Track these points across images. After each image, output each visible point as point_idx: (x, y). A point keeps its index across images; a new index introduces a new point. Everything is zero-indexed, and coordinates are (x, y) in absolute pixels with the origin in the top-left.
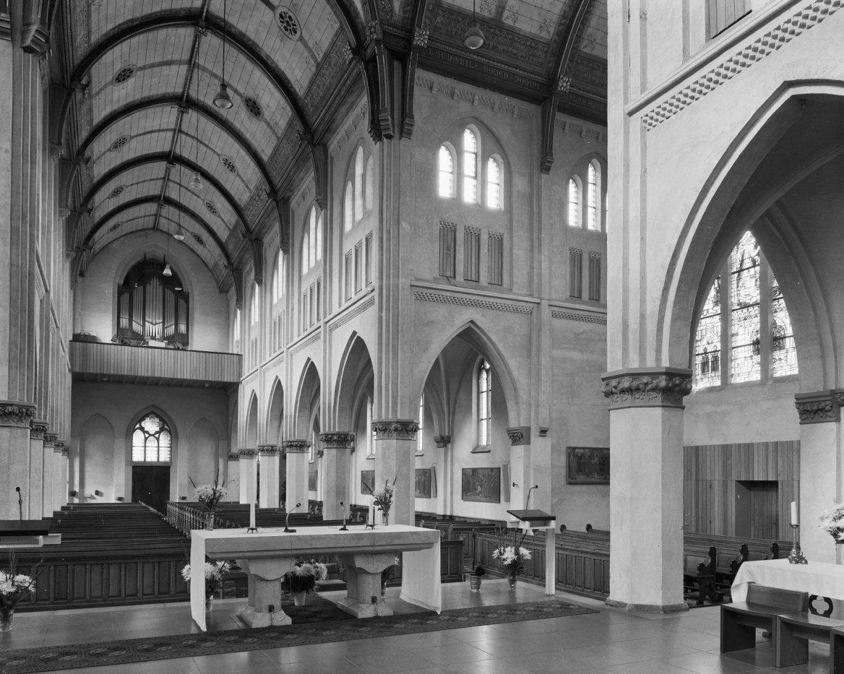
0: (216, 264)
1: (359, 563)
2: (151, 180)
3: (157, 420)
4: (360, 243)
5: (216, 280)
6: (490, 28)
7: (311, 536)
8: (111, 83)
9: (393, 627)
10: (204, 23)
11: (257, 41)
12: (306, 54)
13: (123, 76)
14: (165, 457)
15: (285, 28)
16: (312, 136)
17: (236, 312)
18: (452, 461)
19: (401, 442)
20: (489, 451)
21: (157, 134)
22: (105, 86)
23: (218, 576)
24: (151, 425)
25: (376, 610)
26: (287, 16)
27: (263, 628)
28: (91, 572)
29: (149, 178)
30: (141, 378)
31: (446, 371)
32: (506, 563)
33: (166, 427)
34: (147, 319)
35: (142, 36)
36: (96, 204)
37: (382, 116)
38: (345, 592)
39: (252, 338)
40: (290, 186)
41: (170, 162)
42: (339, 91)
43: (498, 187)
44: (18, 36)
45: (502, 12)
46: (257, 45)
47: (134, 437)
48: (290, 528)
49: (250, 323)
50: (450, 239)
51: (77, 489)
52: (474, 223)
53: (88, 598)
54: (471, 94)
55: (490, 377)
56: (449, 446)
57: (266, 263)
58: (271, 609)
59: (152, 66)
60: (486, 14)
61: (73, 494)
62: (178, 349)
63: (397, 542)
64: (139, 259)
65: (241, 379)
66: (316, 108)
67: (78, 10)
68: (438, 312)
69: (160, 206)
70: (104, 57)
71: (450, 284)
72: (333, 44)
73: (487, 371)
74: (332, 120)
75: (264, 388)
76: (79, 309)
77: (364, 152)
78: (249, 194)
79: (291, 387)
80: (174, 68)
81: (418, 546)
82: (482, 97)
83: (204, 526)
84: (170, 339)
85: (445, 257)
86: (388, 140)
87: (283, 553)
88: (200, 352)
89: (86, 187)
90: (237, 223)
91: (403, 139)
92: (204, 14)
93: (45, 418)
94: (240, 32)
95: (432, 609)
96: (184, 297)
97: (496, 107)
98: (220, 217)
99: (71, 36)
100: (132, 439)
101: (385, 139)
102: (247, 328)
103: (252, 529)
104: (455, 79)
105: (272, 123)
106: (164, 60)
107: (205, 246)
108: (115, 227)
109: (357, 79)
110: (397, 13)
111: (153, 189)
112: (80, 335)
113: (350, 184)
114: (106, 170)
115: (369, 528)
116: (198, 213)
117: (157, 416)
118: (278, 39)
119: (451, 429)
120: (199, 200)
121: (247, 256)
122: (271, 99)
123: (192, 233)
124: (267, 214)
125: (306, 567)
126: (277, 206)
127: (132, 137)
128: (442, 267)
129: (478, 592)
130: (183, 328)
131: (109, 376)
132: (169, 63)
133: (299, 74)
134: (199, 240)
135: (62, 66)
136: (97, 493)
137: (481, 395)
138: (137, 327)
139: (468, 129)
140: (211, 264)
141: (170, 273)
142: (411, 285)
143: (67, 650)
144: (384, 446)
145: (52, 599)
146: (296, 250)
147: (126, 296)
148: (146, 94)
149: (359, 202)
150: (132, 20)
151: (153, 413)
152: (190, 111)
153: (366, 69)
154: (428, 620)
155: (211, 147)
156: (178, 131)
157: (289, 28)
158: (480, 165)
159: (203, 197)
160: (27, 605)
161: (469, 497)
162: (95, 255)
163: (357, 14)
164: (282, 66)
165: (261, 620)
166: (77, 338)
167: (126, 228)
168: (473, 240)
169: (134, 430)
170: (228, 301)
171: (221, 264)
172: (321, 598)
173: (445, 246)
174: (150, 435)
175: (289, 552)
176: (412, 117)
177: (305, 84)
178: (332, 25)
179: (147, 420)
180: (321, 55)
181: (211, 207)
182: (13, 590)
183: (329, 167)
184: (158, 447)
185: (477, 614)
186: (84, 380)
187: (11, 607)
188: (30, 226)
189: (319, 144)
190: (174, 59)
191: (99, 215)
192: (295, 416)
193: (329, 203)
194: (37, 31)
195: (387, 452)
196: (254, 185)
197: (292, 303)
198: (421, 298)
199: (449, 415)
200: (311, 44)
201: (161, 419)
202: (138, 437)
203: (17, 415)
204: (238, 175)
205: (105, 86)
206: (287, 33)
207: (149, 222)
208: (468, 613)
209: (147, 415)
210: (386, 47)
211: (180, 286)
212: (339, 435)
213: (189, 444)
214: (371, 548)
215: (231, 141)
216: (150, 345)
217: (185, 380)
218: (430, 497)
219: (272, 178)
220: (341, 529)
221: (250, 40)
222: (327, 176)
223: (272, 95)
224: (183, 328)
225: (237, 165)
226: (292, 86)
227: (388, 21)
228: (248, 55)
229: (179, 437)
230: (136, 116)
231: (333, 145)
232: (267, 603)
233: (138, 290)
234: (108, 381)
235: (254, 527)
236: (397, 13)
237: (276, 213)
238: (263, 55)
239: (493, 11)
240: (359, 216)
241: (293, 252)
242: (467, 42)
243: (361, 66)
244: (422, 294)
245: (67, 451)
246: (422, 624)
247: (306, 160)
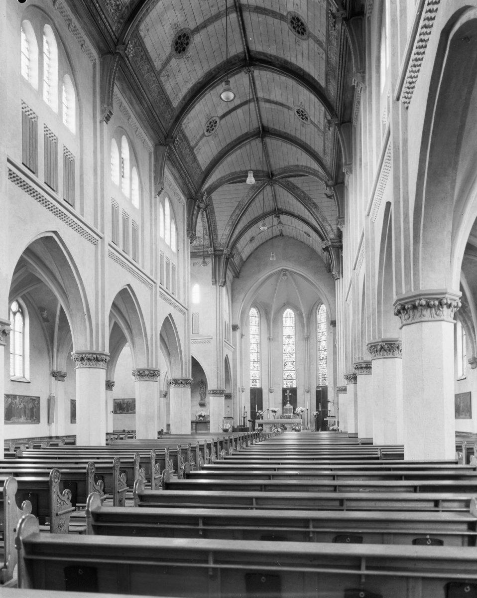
157: (303, 117)
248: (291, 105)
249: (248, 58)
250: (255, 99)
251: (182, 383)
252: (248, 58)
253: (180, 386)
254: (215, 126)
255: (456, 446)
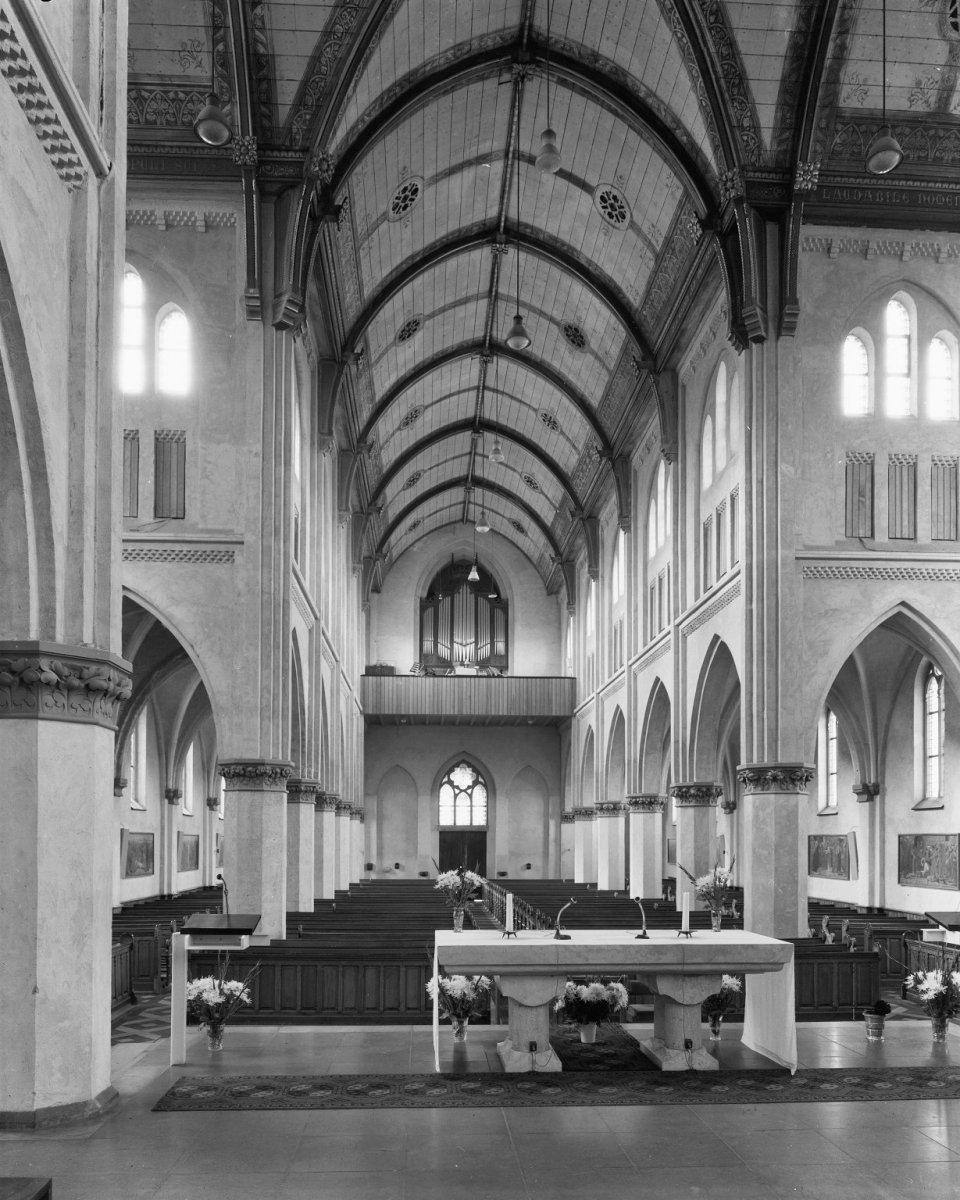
0: (542, 557)
1: (664, 987)
2: (454, 458)
3: (469, 771)
4: (723, 503)
5: (542, 579)
6: (927, 129)
7: (586, 946)
8: (394, 344)
9: (709, 1090)
10: (504, 236)
11: (573, 244)
12: (640, 244)
13: (408, 331)
14: (480, 820)
15: (610, 215)
16: (655, 363)
17: (568, 619)
18: (883, 823)
19: (782, 799)
20: (942, 808)
21: (456, 397)
22: (387, 350)
23: (472, 996)
24: (462, 777)
25: (690, 1059)
26: (611, 196)
27: (520, 1073)
28: (343, 976)
29: (452, 456)
30: (448, 717)
31: (870, 684)
32: (925, 997)
33: (481, 780)
34: (456, 639)
35: (426, 274)
36: (389, 500)
37: (746, 312)
38: (650, 1026)
39: (589, 654)
40: (630, 436)
41: (476, 431)
42: (688, 288)
43: (867, 378)
44: (270, 312)
45: (948, 98)
46: (574, 249)
47: (441, 794)
48: (563, 932)
49: (585, 633)
50: (864, 476)
51: (374, 861)
52: (904, 447)
53: (340, 1008)
54: (898, 243)
55: (943, 687)
56: (878, 799)
57: (603, 547)
58: (533, 1047)
59: (443, 310)
60: (920, 107)
61: (369, 867)
62: (494, 676)
63: (721, 959)
64: (445, 562)
65: (575, 711)
66: (658, 319)
67: (344, 260)
68: (842, 594)
69: (468, 490)
70: (381, 313)
71: (866, 548)
72: (676, 221)
73: (939, 679)
74: (681, 331)
75: (603, 723)
76: (373, 635)
77: (727, 368)
78: (577, 457)
79: (636, 720)
80: (471, 306)
81: (757, 967)
82: (918, 245)
83: (450, 926)
84: (483, 664)
85: (856, 507)
86: (759, 345)
87: (547, 969)
88: (520, 678)
89: (373, 481)
90: (564, 499)
91: (781, 338)
92: (502, 224)
93: (316, 777)
94: (551, 237)
95: (784, 1065)
96: (501, 605)
97: (944, 255)
98: (542, 493)
99: (338, 295)
100: (439, 797)
101: (754, 345)
102: (582, 641)
103: (509, 933)
104: (868, 227)
105: (600, 353)
106: (458, 298)
107: (526, 535)
108: (415, 526)
109: (713, 263)
110: (768, 149)
111: (458, 470)
112: (375, 667)
113: (709, 420)
114: (398, 454)
115: (682, 935)
116: (515, 492)
117: (469, 765)
118: (601, 235)
119: (881, 772)
120: (515, 474)
121: (580, 541)
122: (598, 319)
123: (509, 520)
124: (601, 481)
125: (596, 989)
126: (613, 465)
127: (426, 407)
128: (850, 525)
129: (879, 1043)
130: (500, 646)
131: (407, 716)
132: (466, 301)
133: (632, 276)
134: (519, 528)
135: (330, 336)
136: (397, 866)
137: (929, 717)
138: (444, 651)
139: (895, 299)
140: (535, 557)
141: (477, 577)
142: (797, 558)
143: (266, 1082)
144: (757, 804)
145: (299, 1008)
146: (640, 525)
147: (430, 611)
148: (438, 348)
149: (721, 442)
150: (412, 257)
151: (464, 761)
152: (495, 358)
153: (724, 246)
154: (769, 1083)
155: (525, 399)
156: (481, 388)
157: (614, 213)
158: (915, 354)
159: (520, 470)
160: (271, 1013)
161: (909, 880)
162: (392, 564)
163: (707, 164)
164: (609, 270)
165: (517, 1061)
166: (373, 671)
167: (429, 524)
168: (905, 473)
169: (441, 785)
170: (558, 604)
171: (547, 556)
172: (624, 1032)
173: (856, 490)
174: (461, 791)
175: (555, 969)
176: (796, 302)
177: (642, 288)
178: (672, 193)
179: (458, 771)
180: (661, 243)
181: (530, 482)
182: (221, 1000)
183: (680, 399)
184: (471, 806)
185: (857, 1080)
186: (380, 724)
187: (220, 1021)
188: (284, 542)
189: (664, 369)
190: (470, 294)
191: (392, 513)
192: (641, 761)
193: (680, 453)
194: (289, 301)
195: (761, 813)
196: (582, 443)
197: (636, 601)
198: (814, 576)
199: (877, 751)
200: (645, 229)
201: (475, 770)
202: (446, 792)
203: (270, 776)
204: (562, 433)
205: (387, 350)
206: (612, 221)
207: (456, 512)
208: (844, 1077)
209: (457, 765)
210: (751, 206)
211: (497, 590)
212: (698, 787)
213: (510, 801)
214: (680, 968)
215: (550, 387)
216: (458, 673)
217: (502, 717)
218: (849, 879)
219: (606, 430)
220: (639, 937)
221: (564, 244)
222: (677, 414)
223: (599, 314)
224: (500, 646)
225: (560, 420)
226: (624, 294)
227: (753, 164)
228: (563, 266)
229: (498, 792)
230: (428, 378)
231: (685, 368)
232: (526, 1039)
233: (445, 603)
234: (409, 723)
235: (512, 930)
236: (768, 149)
237: (612, 480)
238: (583, 261)
239: (933, 100)
240: (721, 464)
241: (636, 528)
242: (872, 164)
243: (716, 245)
244: (817, 568)
245: (360, 814)
246: (757, 1089)
247: (648, 396)
248: (592, 180)
249: (525, 41)
250: (510, 155)
251: (775, 779)
252: (525, 41)
253: (772, 790)
254: (412, 200)
255: (114, 915)
